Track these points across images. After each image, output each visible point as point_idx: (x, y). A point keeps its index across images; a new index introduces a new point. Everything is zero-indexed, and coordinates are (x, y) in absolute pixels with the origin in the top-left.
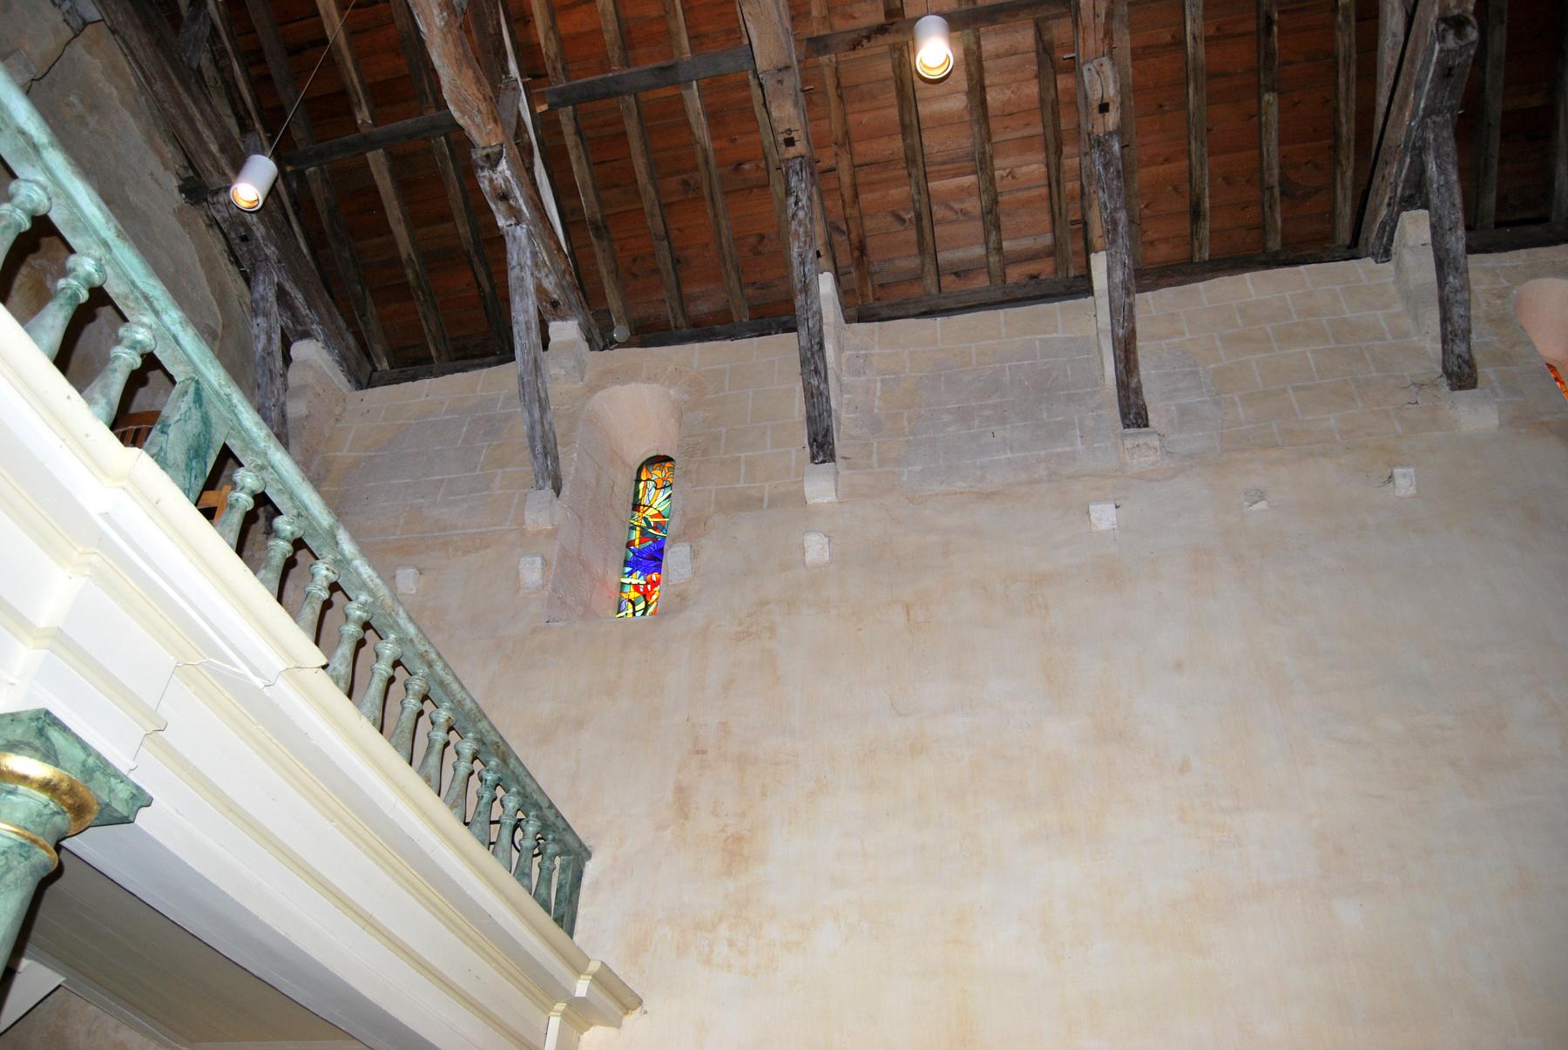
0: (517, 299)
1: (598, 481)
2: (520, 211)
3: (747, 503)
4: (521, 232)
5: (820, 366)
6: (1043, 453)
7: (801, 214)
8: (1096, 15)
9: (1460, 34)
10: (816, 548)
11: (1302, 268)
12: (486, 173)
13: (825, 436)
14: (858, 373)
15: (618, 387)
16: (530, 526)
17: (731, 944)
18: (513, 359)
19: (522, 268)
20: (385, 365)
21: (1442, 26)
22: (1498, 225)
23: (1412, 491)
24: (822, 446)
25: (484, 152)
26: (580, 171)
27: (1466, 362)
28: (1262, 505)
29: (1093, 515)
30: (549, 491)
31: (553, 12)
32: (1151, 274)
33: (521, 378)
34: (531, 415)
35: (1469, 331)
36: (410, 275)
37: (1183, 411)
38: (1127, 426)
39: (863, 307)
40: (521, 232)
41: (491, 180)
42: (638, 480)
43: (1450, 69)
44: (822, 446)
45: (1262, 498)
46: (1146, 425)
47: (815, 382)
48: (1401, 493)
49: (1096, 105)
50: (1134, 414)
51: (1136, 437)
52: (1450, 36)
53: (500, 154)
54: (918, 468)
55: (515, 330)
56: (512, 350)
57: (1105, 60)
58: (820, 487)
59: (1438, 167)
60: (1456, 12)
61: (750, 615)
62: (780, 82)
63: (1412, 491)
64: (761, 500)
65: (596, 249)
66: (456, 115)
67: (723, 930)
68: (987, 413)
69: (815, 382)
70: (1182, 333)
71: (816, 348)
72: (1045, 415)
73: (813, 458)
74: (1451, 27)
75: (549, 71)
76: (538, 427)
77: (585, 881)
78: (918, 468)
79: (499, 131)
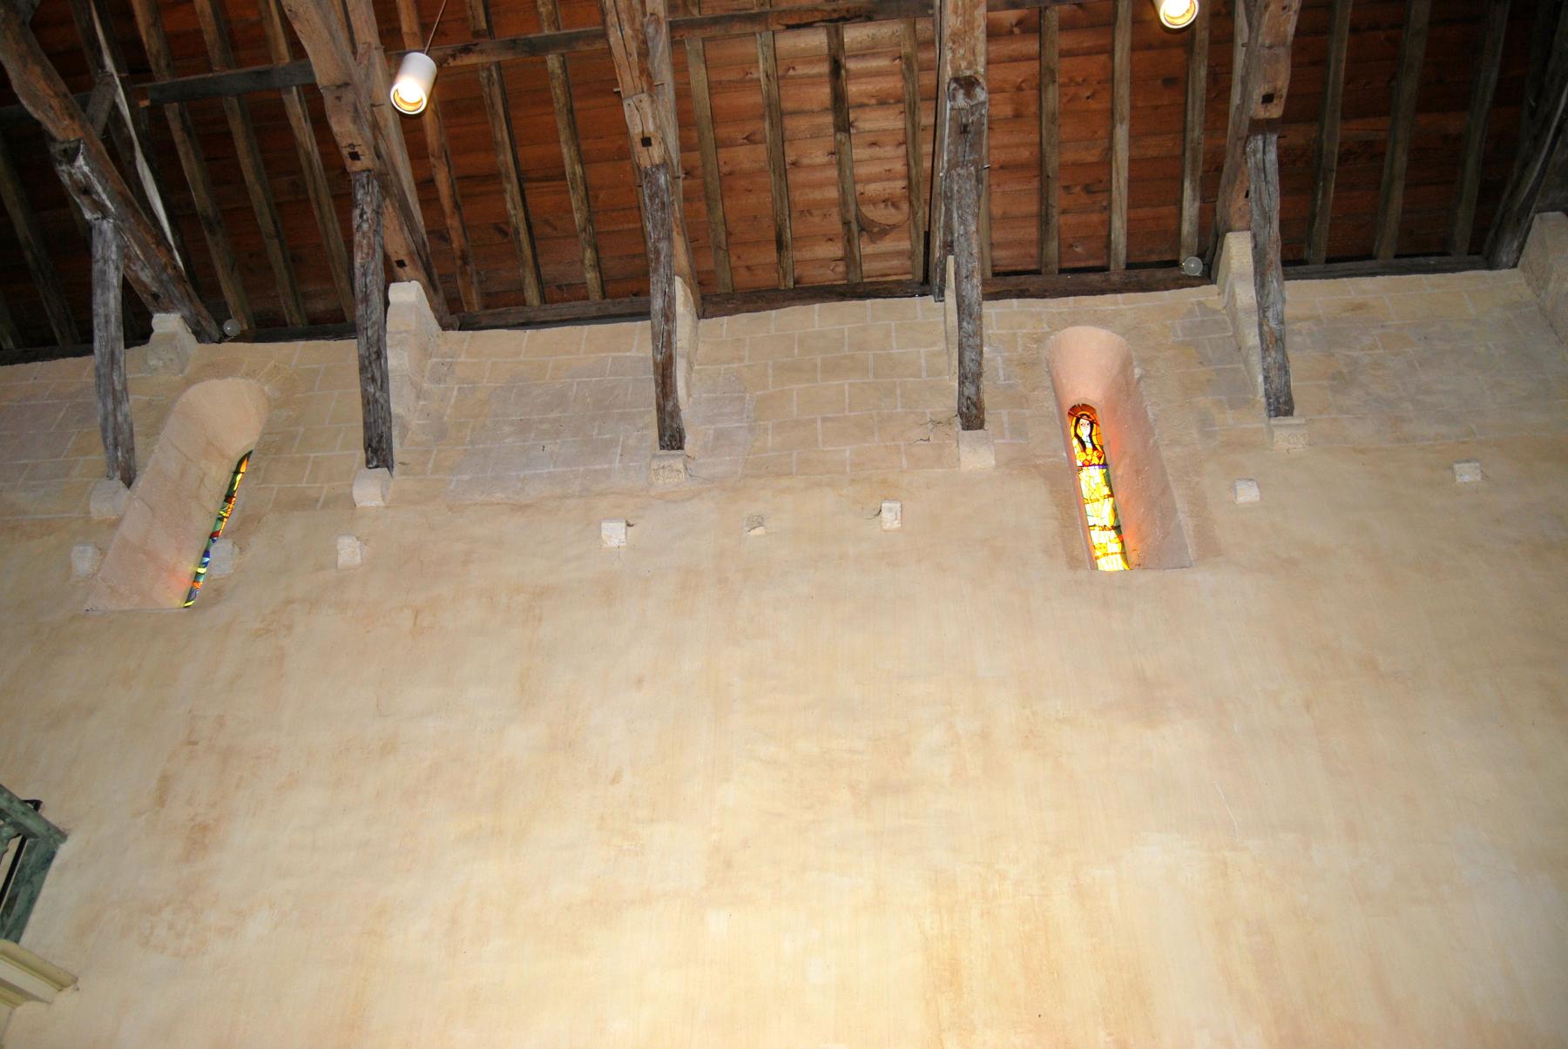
0: (99, 292)
1: (183, 473)
2: (104, 206)
3: (302, 503)
4: (107, 226)
5: (377, 375)
6: (582, 469)
7: (365, 226)
8: (628, 54)
9: (969, 94)
10: (349, 551)
11: (868, 302)
12: (64, 167)
13: (379, 442)
14: (439, 381)
15: (215, 381)
16: (95, 515)
17: (171, 926)
18: (90, 352)
19: (106, 262)
20: (11, 344)
21: (953, 85)
22: (1062, 271)
23: (896, 524)
24: (378, 452)
25: (63, 147)
26: (191, 166)
27: (974, 404)
28: (759, 531)
29: (604, 533)
30: (117, 483)
31: (158, 11)
32: (1008, 282)
33: (97, 369)
34: (105, 406)
35: (980, 375)
36: (29, 257)
37: (720, 435)
38: (662, 448)
39: (714, 300)
40: (107, 226)
41: (70, 175)
42: (237, 472)
43: (966, 126)
44: (378, 452)
45: (761, 524)
46: (681, 448)
47: (371, 389)
48: (887, 526)
49: (637, 140)
50: (672, 438)
51: (675, 460)
52: (960, 95)
53: (78, 149)
54: (466, 477)
55: (95, 322)
56: (90, 341)
57: (644, 97)
58: (369, 490)
59: (960, 217)
60: (968, 73)
61: (274, 612)
62: (339, 98)
63: (896, 524)
64: (317, 501)
65: (210, 242)
66: (30, 109)
67: (167, 914)
68: (545, 426)
69: (371, 389)
70: (741, 359)
71: (374, 356)
72: (595, 432)
73: (368, 462)
74: (962, 86)
75: (153, 67)
76: (111, 419)
77: (56, 862)
78: (466, 477)
79: (76, 127)
